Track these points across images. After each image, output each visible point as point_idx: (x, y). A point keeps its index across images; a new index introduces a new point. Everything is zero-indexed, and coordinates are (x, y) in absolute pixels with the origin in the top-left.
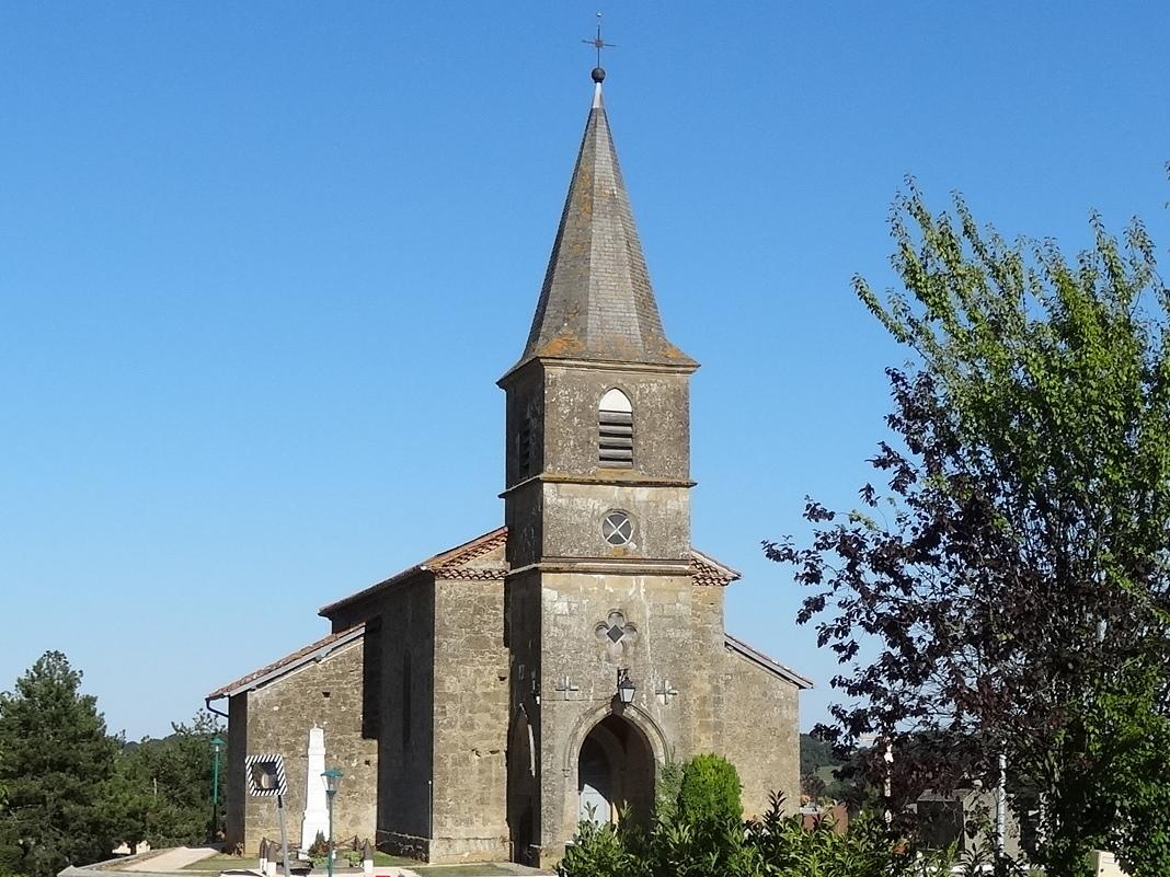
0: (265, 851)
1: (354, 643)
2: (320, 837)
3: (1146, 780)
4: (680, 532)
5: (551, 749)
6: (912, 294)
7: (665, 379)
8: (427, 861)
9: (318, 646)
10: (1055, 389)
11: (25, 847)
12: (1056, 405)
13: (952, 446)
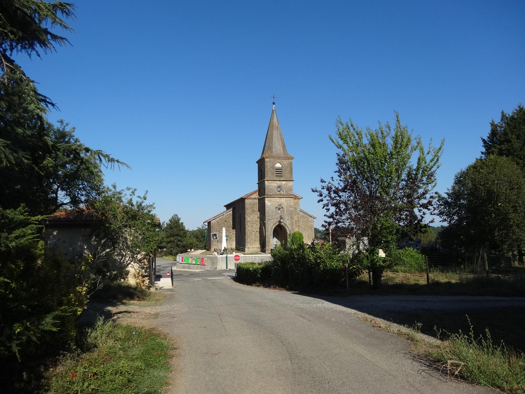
0: (215, 251)
1: (230, 212)
2: (225, 248)
3: (390, 235)
4: (291, 190)
5: (268, 231)
6: (340, 139)
7: (288, 161)
8: (245, 252)
9: (224, 212)
10: (370, 157)
11: (171, 250)
12: (370, 160)
13: (349, 169)
